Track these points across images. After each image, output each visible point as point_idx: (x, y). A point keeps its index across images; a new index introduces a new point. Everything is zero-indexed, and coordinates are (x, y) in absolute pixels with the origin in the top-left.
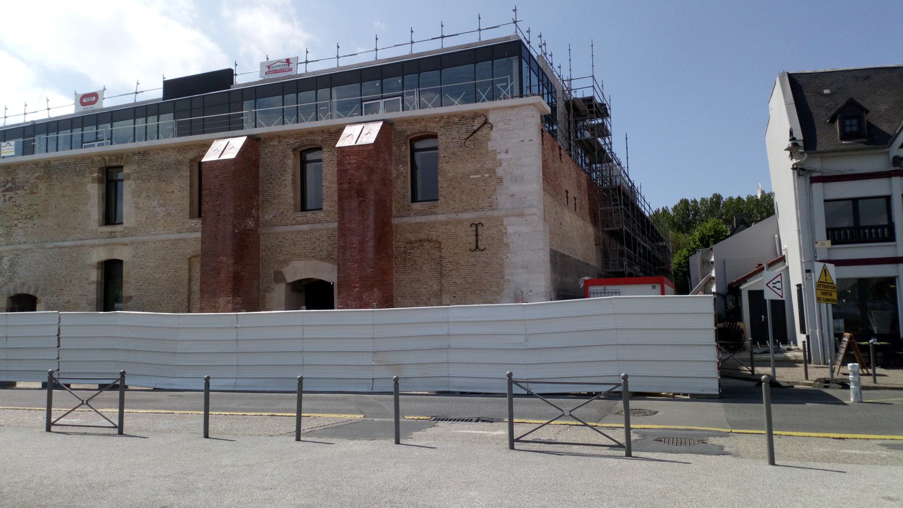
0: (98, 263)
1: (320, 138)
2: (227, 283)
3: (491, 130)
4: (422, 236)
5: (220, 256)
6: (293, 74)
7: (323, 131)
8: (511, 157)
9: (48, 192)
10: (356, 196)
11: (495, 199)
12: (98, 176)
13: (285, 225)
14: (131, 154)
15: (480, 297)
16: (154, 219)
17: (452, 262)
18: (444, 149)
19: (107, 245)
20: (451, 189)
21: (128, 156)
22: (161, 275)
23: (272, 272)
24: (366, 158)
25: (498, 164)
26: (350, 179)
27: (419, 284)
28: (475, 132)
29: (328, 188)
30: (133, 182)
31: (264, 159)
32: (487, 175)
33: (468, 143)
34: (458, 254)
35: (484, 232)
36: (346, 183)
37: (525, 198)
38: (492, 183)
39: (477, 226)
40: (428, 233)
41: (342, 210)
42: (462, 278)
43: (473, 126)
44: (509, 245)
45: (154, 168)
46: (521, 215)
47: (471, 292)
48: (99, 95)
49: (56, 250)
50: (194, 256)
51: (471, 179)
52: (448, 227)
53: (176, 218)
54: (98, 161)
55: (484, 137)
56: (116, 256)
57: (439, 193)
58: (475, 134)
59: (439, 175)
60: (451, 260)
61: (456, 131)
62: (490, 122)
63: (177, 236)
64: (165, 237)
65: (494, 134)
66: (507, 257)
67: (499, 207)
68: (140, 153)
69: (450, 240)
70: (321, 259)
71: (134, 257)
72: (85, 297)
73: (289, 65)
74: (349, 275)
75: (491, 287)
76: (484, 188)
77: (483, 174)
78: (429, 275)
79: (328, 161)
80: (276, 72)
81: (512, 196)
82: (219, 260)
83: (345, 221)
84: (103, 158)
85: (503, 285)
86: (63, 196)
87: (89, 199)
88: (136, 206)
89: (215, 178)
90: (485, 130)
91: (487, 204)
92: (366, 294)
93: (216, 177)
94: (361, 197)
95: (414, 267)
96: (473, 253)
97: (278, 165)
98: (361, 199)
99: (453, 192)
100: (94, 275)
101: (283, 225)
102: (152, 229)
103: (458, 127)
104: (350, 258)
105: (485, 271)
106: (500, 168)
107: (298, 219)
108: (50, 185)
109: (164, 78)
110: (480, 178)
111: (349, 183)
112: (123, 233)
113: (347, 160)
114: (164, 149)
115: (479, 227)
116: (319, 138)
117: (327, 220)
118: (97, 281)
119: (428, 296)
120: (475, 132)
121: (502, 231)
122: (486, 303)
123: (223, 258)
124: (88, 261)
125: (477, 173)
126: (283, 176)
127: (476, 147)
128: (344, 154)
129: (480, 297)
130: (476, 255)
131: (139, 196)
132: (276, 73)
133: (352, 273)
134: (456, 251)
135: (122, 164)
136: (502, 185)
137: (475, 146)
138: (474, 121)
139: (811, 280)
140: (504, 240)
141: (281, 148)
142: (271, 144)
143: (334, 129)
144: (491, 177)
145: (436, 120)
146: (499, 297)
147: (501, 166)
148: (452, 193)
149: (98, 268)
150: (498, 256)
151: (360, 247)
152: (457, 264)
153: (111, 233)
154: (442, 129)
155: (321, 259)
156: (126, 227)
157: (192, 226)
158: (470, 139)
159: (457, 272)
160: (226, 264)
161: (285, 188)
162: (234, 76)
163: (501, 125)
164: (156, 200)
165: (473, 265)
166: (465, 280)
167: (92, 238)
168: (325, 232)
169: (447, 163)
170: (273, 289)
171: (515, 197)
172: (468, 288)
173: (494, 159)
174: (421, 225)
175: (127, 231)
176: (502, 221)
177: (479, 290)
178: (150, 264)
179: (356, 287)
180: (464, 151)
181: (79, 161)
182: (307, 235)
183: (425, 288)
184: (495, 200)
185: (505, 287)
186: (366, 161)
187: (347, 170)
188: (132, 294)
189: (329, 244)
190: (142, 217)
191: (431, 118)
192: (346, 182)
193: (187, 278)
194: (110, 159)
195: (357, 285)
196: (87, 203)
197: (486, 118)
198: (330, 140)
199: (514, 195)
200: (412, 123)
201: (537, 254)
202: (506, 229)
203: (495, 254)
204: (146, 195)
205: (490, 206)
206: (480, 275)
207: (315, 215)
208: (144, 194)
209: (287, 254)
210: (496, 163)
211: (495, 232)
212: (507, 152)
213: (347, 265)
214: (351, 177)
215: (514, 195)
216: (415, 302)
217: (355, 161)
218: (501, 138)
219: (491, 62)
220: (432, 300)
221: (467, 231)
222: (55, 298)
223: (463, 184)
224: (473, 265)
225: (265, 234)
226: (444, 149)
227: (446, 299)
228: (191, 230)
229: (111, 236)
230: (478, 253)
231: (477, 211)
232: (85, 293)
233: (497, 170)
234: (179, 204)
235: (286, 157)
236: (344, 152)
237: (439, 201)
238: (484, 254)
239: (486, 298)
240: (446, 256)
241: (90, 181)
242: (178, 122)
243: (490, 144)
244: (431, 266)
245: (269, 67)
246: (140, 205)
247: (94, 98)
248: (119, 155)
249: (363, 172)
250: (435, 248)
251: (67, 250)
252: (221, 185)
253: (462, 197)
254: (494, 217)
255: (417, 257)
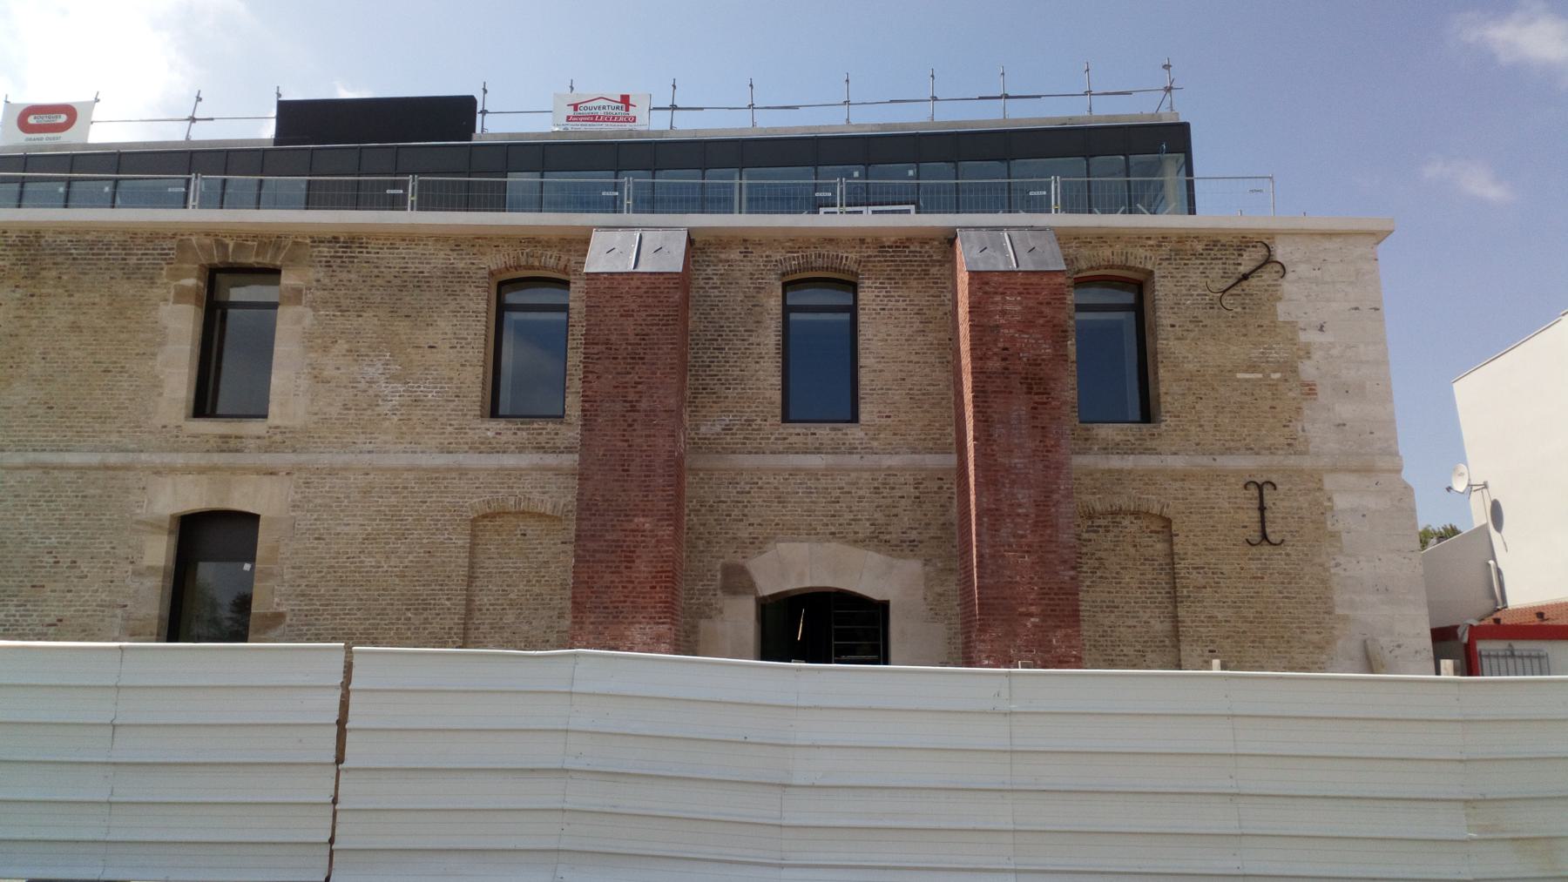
0: (173, 517)
1: (853, 256)
2: (654, 587)
3: (1282, 277)
4: (1122, 501)
5: (635, 516)
6: (639, 128)
7: (862, 241)
8: (1332, 340)
9: (23, 312)
10: (1025, 390)
11: (1300, 428)
12: (198, 287)
13: (756, 453)
14: (308, 241)
15: (1276, 655)
16: (369, 412)
17: (1203, 568)
18: (1172, 308)
19: (214, 468)
20: (1191, 399)
21: (296, 243)
22: (383, 560)
23: (718, 567)
24: (1049, 303)
25: (1301, 353)
26: (1005, 349)
27: (1113, 615)
28: (1245, 277)
29: (875, 371)
30: (310, 313)
31: (701, 291)
32: (1277, 376)
33: (1227, 301)
34: (1216, 549)
35: (1277, 502)
36: (995, 358)
37: (1372, 433)
38: (1291, 394)
39: (1260, 487)
40: (1139, 495)
41: (986, 421)
42: (1229, 607)
43: (1240, 264)
44: (1340, 536)
45: (379, 281)
46: (1367, 470)
47: (1253, 642)
48: (16, 127)
49: (34, 474)
50: (485, 516)
51: (1238, 380)
52: (1187, 485)
53: (437, 413)
54: (202, 247)
55: (1266, 290)
56: (238, 501)
57: (1162, 406)
58: (1245, 283)
59: (1160, 365)
60: (1198, 562)
61: (1198, 271)
62: (1279, 259)
63: (442, 460)
64: (403, 460)
65: (1288, 287)
66: (1337, 565)
67: (1310, 447)
68: (335, 239)
69: (1194, 517)
70: (856, 541)
71: (295, 506)
72: (119, 612)
73: (627, 110)
74: (1010, 582)
75: (1304, 632)
76: (1270, 403)
77: (1267, 371)
78: (1139, 595)
79: (874, 310)
80: (594, 119)
81: (1339, 425)
82: (632, 526)
83: (995, 447)
84: (217, 241)
85: (1333, 628)
86: (75, 328)
87: (161, 344)
88: (316, 372)
89: (621, 316)
90: (1267, 276)
91: (1282, 439)
92: (1060, 633)
93: (627, 314)
94: (1037, 394)
95: (1099, 574)
96: (1254, 549)
97: (739, 308)
98: (1036, 398)
99: (1197, 406)
100: (159, 551)
101: (750, 453)
102: (362, 436)
103: (1202, 264)
104: (1012, 540)
105: (1286, 594)
106: (1307, 362)
107: (792, 439)
108: (32, 296)
109: (279, 95)
110: (1260, 379)
111: (1004, 359)
112: (266, 442)
113: (997, 303)
114: (410, 237)
115: (1267, 490)
116: (851, 257)
117: (872, 448)
118: (165, 567)
119: (1139, 647)
120: (1245, 277)
121: (1321, 504)
122: (1292, 669)
123: (642, 520)
124: (138, 511)
125: (1252, 368)
126: (754, 334)
127: (1247, 311)
128: (987, 288)
129: (1276, 655)
130: (1262, 554)
131: (326, 349)
132: (594, 121)
133: (1018, 578)
134: (1209, 542)
135: (278, 263)
136: (1315, 399)
137: (1244, 308)
138: (1241, 255)
139: (1035, 662)
140: (1329, 523)
141: (749, 268)
142: (723, 256)
143: (893, 239)
144: (1286, 380)
145: (1151, 242)
146: (1324, 656)
147: (1309, 358)
148: (1194, 408)
149: (170, 532)
150: (1317, 560)
151: (1037, 516)
152: (1213, 573)
153: (225, 438)
154: (1165, 263)
155: (856, 541)
156: (277, 427)
157: (487, 438)
158: (1232, 291)
159: (1216, 592)
160: (653, 537)
161: (757, 362)
162: (479, 117)
163: (1303, 269)
164: (379, 365)
165: (1254, 578)
166: (1237, 612)
167: (161, 450)
168: (866, 475)
169: (1179, 339)
170: (721, 611)
171: (1347, 427)
172: (1244, 632)
173: (1292, 341)
174: (1119, 476)
175: (278, 438)
176: (1320, 480)
177: (1272, 637)
178: (347, 529)
179: (1031, 615)
180: (1219, 317)
181: (139, 241)
182: (818, 480)
183: (1130, 627)
184: (1301, 433)
185: (1336, 633)
186: (1047, 310)
187: (997, 326)
188: (282, 609)
189: (877, 507)
190: (330, 405)
191: (1140, 237)
192: (995, 354)
193: (464, 571)
194: (240, 247)
195: (1033, 609)
196: (154, 355)
197: (1269, 251)
198: (880, 261)
199: (1344, 425)
200: (1090, 243)
201: (1406, 561)
202: (1330, 499)
203: (1307, 555)
204: (346, 346)
205: (1288, 444)
206: (1274, 603)
207: (840, 433)
208: (342, 346)
209: (760, 525)
210: (1298, 349)
211: (1306, 505)
212: (1321, 329)
213: (1003, 556)
214: (1007, 345)
215: (1344, 425)
216: (1105, 660)
217: (1018, 308)
218: (1306, 296)
219: (1122, 158)
220: (1150, 656)
221: (1236, 498)
222: (13, 608)
223: (1222, 390)
224: (1254, 578)
225: (700, 470)
226: (1172, 308)
227: (1191, 656)
228: (482, 447)
229: (225, 446)
230: (1266, 549)
231: (1258, 454)
232: (120, 601)
233: (1301, 366)
234: (451, 379)
235: (763, 291)
236: (987, 283)
237: (1163, 424)
238: (1280, 554)
239: (1293, 658)
240: (1186, 554)
241: (171, 296)
242: (420, 181)
243: (1281, 307)
244: (1141, 574)
245: (576, 107)
246: (326, 373)
247: (63, 118)
248: (271, 240)
249: (1039, 336)
250: (1151, 532)
251: (72, 475)
252: (643, 336)
253: (1219, 420)
254: (1302, 471)
255: (1106, 550)
